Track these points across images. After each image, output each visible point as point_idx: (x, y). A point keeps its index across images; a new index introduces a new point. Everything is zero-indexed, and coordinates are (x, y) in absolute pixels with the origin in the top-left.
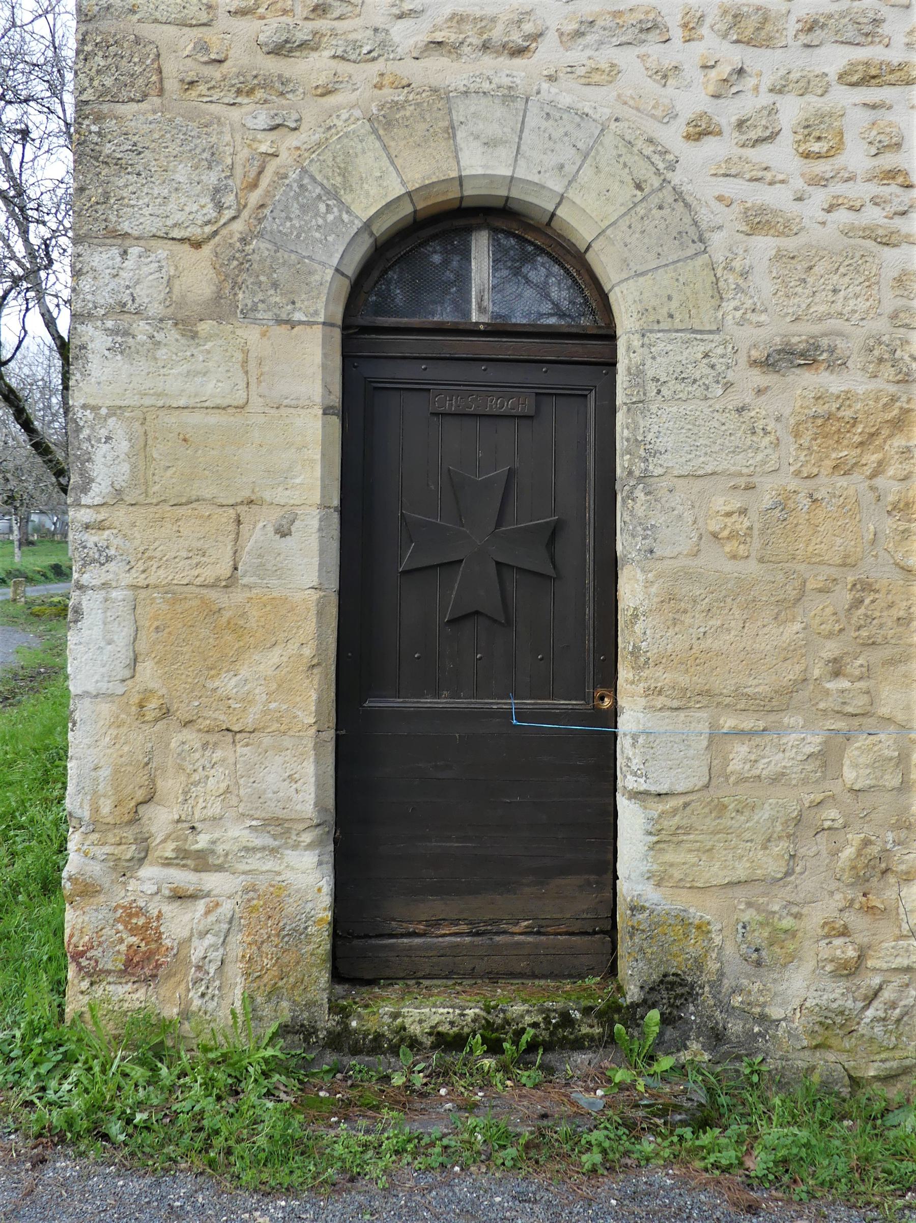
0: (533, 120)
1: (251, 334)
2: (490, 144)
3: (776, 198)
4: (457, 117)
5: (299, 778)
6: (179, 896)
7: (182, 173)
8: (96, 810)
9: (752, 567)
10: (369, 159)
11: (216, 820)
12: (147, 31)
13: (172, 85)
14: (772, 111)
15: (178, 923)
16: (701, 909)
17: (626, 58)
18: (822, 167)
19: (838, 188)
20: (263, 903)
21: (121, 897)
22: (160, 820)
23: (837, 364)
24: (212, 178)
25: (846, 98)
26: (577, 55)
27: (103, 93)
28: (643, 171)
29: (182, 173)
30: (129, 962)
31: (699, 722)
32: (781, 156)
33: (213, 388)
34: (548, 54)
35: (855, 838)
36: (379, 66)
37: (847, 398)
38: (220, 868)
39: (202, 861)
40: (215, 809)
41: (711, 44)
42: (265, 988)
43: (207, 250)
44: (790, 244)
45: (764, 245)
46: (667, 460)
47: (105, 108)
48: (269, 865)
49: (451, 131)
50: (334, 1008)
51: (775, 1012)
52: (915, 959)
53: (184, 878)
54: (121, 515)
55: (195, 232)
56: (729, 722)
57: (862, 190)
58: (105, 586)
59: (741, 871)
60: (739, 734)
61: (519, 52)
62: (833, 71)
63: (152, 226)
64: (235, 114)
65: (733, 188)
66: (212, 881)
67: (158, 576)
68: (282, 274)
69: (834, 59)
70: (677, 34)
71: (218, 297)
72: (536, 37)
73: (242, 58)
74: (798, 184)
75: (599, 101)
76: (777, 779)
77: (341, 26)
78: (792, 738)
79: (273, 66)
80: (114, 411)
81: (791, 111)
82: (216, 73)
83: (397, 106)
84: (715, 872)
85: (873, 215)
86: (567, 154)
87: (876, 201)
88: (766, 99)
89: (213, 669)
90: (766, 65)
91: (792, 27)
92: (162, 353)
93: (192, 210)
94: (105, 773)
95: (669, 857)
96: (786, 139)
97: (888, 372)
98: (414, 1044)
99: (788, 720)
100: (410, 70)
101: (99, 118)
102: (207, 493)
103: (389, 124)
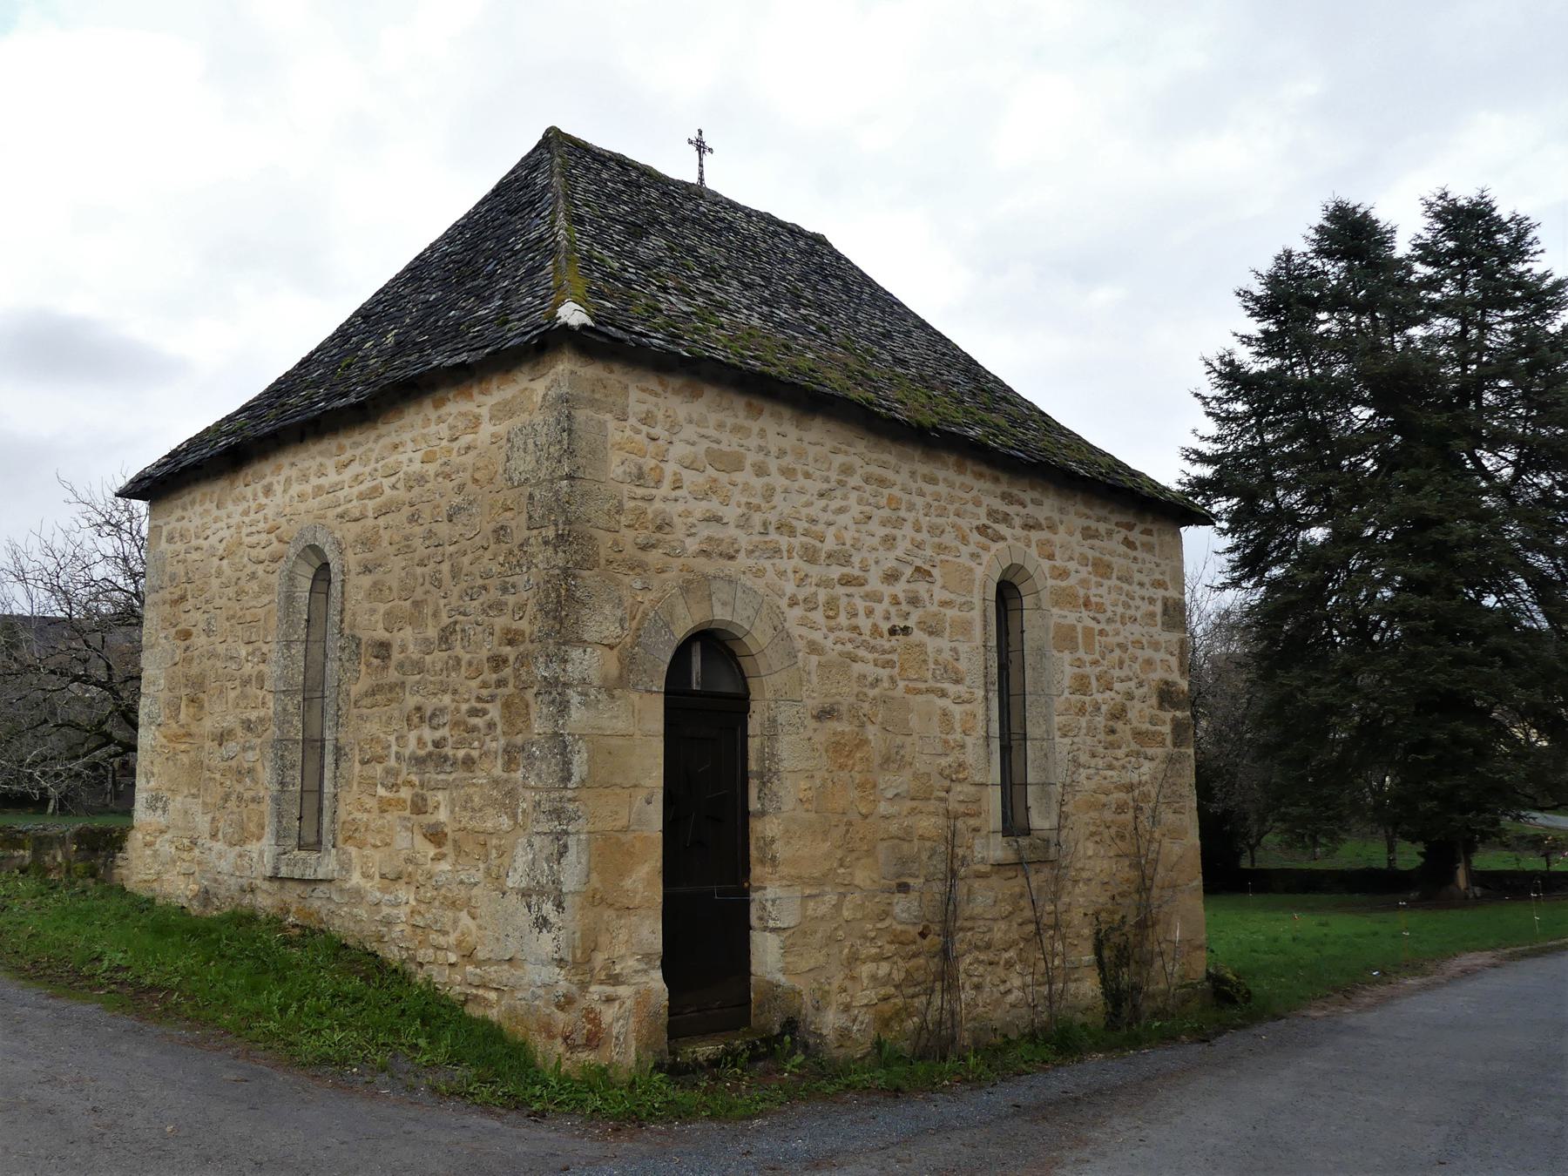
0: (739, 594)
1: (635, 697)
2: (724, 604)
3: (817, 636)
4: (713, 589)
5: (651, 932)
6: (609, 1000)
7: (607, 609)
8: (574, 956)
9: (813, 815)
10: (680, 609)
11: (622, 957)
12: (594, 532)
13: (603, 562)
14: (816, 594)
15: (608, 1014)
16: (799, 984)
17: (767, 564)
18: (833, 623)
19: (838, 633)
20: (642, 998)
21: (583, 1003)
22: (599, 958)
23: (839, 719)
24: (619, 613)
25: (841, 590)
26: (751, 562)
27: (576, 564)
28: (776, 622)
29: (607, 609)
30: (588, 1039)
31: (797, 891)
32: (818, 616)
33: (621, 725)
34: (742, 561)
35: (848, 944)
36: (682, 560)
37: (843, 733)
38: (623, 983)
39: (615, 980)
40: (623, 951)
41: (796, 561)
42: (644, 1046)
43: (615, 651)
44: (823, 659)
45: (814, 659)
46: (785, 764)
47: (577, 572)
48: (644, 979)
49: (710, 596)
50: (671, 1053)
51: (825, 1032)
52: (1565, 863)
53: (609, 990)
54: (584, 793)
55: (611, 641)
56: (808, 892)
57: (846, 635)
58: (578, 832)
59: (812, 964)
60: (810, 896)
61: (732, 558)
62: (836, 576)
63: (596, 637)
64: (627, 580)
65: (804, 631)
66: (622, 991)
67: (599, 826)
68: (648, 666)
69: (836, 572)
70: (785, 554)
71: (621, 676)
72: (737, 551)
73: (630, 550)
74: (825, 630)
75: (760, 585)
76: (823, 918)
77: (668, 537)
78: (826, 898)
79: (640, 555)
80: (581, 737)
81: (822, 596)
82: (619, 557)
83: (689, 582)
84: (804, 965)
85: (849, 647)
86: (750, 612)
87: (851, 641)
88: (814, 589)
89: (622, 876)
90: (815, 571)
91: (823, 555)
92: (600, 706)
93: (611, 630)
94: (578, 935)
95: (789, 959)
96: (821, 608)
97: (856, 722)
98: (701, 1066)
99: (827, 889)
100: (692, 562)
101: (575, 577)
102: (618, 781)
103: (687, 591)
